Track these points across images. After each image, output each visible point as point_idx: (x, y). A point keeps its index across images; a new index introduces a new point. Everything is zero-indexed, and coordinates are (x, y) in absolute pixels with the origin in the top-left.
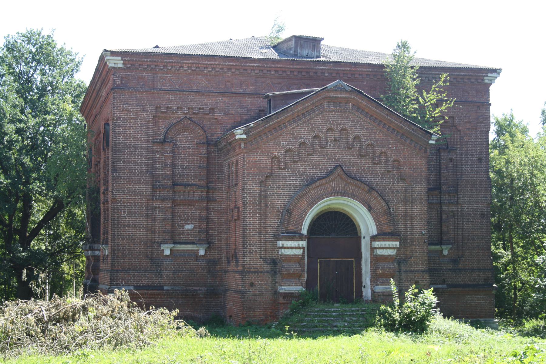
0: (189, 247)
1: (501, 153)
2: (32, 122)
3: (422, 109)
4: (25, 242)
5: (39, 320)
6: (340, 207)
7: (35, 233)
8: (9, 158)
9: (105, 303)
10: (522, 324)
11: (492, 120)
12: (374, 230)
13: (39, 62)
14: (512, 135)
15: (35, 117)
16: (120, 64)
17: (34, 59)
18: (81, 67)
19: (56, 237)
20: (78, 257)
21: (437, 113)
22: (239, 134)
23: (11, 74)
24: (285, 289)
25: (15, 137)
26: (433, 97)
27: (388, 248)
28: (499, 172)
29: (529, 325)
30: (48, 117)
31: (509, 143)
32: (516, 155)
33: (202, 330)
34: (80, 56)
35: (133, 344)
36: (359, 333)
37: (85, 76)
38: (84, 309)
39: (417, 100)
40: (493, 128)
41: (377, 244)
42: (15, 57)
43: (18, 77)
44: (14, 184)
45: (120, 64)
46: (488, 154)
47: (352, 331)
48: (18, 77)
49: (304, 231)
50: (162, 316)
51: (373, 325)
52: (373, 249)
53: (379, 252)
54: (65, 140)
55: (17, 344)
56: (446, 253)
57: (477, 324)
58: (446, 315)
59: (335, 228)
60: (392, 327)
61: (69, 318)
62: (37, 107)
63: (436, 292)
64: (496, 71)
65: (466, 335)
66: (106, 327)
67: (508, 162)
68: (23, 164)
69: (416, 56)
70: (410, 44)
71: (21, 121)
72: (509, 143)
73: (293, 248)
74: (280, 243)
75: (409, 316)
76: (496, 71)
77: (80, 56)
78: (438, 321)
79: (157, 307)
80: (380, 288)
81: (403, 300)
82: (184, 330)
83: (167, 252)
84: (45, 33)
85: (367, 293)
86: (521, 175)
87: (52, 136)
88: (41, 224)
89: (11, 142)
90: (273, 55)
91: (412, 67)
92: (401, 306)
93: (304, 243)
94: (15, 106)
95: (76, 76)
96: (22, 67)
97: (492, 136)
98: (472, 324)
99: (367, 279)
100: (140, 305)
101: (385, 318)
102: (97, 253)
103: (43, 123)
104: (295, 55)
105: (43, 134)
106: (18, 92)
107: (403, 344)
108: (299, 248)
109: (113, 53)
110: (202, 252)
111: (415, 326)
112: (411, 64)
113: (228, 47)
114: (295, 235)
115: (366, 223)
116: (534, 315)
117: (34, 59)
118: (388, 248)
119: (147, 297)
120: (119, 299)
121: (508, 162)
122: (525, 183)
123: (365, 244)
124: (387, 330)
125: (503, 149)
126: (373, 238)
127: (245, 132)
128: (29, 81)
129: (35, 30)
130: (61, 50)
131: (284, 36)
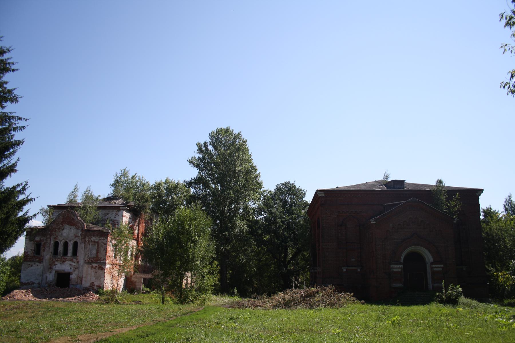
0: (354, 268)
1: (487, 225)
2: (288, 218)
3: (449, 209)
4: (286, 266)
5: (301, 296)
6: (426, 257)
7: (289, 262)
8: (279, 233)
9: (325, 290)
10: (503, 302)
11: (481, 210)
12: (432, 260)
13: (289, 194)
14: (491, 217)
15: (288, 216)
16: (323, 195)
17: (287, 193)
18: (306, 195)
19: (298, 264)
20: (306, 272)
21: (456, 209)
22: (373, 221)
23: (279, 199)
24: (394, 285)
25: (281, 224)
26: (454, 203)
27: (438, 267)
28: (487, 233)
29: (506, 302)
30: (294, 216)
31: (490, 220)
32: (494, 226)
33: (363, 301)
34: (305, 191)
35: (337, 306)
36: (428, 304)
37: (309, 198)
38: (318, 292)
39: (447, 204)
40: (482, 214)
41: (434, 266)
42: (280, 193)
43: (281, 200)
44: (281, 243)
45: (323, 195)
46: (481, 226)
47: (423, 304)
48: (281, 200)
49: (402, 261)
50: (346, 295)
51: (433, 301)
52: (432, 268)
53: (435, 269)
54: (300, 225)
55: (295, 305)
56: (464, 269)
57: (481, 301)
58: (466, 297)
59: (415, 259)
60: (442, 301)
61: (313, 295)
62: (290, 212)
63: (462, 287)
64: (481, 191)
65: (476, 305)
66: (326, 299)
67: (490, 229)
68: (284, 235)
69: (446, 185)
70: (443, 180)
71: (283, 218)
72: (490, 220)
73: (397, 268)
74: (392, 266)
75: (450, 297)
76: (481, 191)
77: (305, 191)
78: (463, 299)
79: (345, 292)
80: (436, 285)
81: (446, 291)
82: (356, 301)
83: (345, 270)
84: (291, 183)
85: (430, 287)
86: (497, 234)
87: (295, 223)
88: (291, 259)
89: (280, 226)
90: (385, 188)
91: (444, 191)
92: (446, 292)
93: (401, 266)
94: (281, 212)
95: (304, 199)
96: (283, 196)
97: (482, 217)
98: (478, 301)
99: (430, 281)
100: (338, 291)
101: (439, 298)
102: (316, 271)
103: (291, 219)
104: (394, 188)
105: (292, 223)
106: (282, 206)
107: (446, 309)
108: (400, 268)
109: (320, 191)
110: (359, 270)
111: (453, 301)
112: (443, 189)
113: (366, 186)
114: (398, 263)
115: (429, 257)
116: (509, 297)
117: (287, 193)
118: (438, 267)
119: (340, 288)
120: (328, 289)
121: (490, 229)
122: (499, 238)
123: (428, 266)
124: (440, 303)
125: (487, 223)
126: (432, 264)
127: (375, 221)
128: (286, 201)
129: (253, 161)
130: (298, 189)
131: (390, 180)
